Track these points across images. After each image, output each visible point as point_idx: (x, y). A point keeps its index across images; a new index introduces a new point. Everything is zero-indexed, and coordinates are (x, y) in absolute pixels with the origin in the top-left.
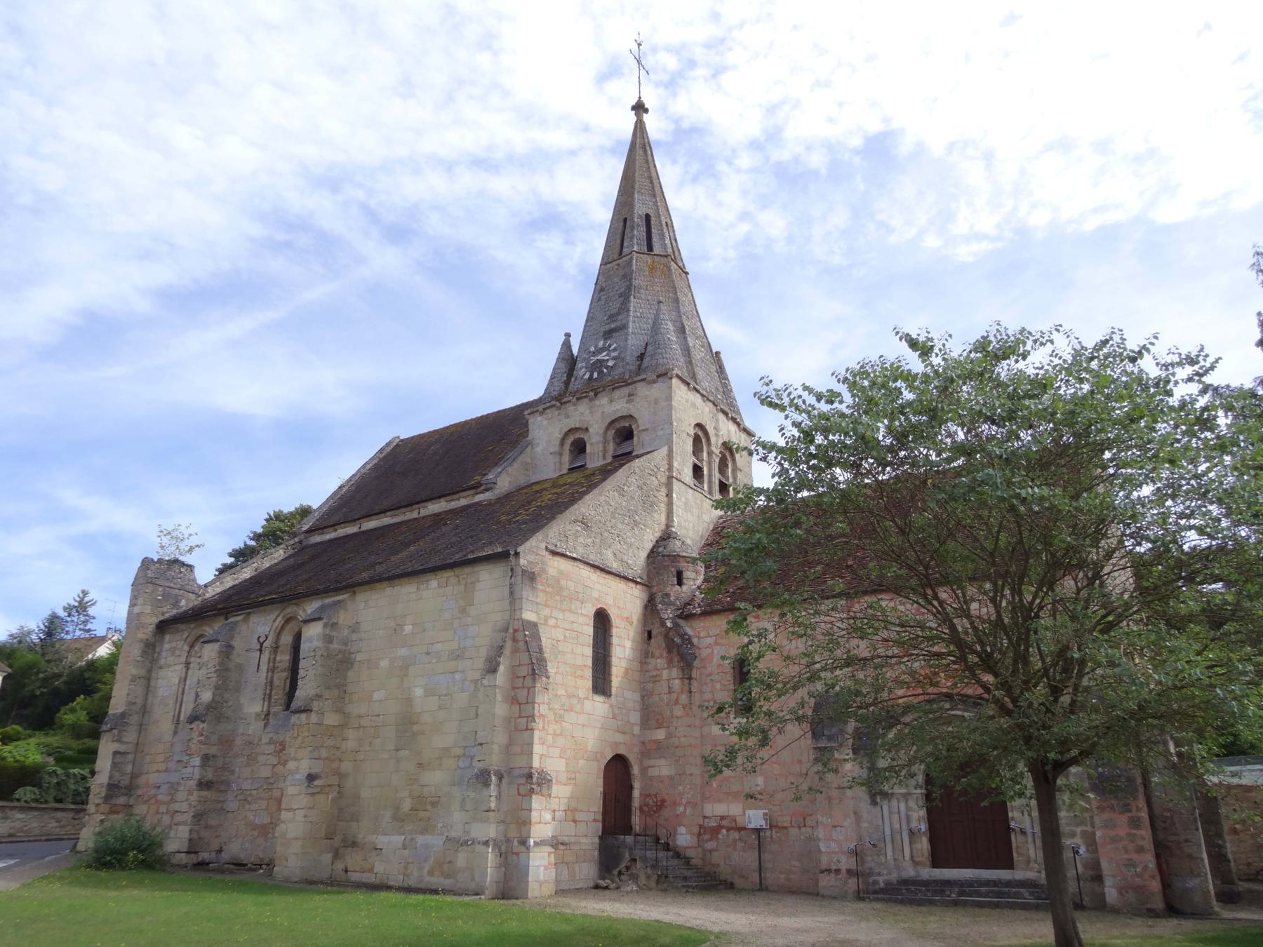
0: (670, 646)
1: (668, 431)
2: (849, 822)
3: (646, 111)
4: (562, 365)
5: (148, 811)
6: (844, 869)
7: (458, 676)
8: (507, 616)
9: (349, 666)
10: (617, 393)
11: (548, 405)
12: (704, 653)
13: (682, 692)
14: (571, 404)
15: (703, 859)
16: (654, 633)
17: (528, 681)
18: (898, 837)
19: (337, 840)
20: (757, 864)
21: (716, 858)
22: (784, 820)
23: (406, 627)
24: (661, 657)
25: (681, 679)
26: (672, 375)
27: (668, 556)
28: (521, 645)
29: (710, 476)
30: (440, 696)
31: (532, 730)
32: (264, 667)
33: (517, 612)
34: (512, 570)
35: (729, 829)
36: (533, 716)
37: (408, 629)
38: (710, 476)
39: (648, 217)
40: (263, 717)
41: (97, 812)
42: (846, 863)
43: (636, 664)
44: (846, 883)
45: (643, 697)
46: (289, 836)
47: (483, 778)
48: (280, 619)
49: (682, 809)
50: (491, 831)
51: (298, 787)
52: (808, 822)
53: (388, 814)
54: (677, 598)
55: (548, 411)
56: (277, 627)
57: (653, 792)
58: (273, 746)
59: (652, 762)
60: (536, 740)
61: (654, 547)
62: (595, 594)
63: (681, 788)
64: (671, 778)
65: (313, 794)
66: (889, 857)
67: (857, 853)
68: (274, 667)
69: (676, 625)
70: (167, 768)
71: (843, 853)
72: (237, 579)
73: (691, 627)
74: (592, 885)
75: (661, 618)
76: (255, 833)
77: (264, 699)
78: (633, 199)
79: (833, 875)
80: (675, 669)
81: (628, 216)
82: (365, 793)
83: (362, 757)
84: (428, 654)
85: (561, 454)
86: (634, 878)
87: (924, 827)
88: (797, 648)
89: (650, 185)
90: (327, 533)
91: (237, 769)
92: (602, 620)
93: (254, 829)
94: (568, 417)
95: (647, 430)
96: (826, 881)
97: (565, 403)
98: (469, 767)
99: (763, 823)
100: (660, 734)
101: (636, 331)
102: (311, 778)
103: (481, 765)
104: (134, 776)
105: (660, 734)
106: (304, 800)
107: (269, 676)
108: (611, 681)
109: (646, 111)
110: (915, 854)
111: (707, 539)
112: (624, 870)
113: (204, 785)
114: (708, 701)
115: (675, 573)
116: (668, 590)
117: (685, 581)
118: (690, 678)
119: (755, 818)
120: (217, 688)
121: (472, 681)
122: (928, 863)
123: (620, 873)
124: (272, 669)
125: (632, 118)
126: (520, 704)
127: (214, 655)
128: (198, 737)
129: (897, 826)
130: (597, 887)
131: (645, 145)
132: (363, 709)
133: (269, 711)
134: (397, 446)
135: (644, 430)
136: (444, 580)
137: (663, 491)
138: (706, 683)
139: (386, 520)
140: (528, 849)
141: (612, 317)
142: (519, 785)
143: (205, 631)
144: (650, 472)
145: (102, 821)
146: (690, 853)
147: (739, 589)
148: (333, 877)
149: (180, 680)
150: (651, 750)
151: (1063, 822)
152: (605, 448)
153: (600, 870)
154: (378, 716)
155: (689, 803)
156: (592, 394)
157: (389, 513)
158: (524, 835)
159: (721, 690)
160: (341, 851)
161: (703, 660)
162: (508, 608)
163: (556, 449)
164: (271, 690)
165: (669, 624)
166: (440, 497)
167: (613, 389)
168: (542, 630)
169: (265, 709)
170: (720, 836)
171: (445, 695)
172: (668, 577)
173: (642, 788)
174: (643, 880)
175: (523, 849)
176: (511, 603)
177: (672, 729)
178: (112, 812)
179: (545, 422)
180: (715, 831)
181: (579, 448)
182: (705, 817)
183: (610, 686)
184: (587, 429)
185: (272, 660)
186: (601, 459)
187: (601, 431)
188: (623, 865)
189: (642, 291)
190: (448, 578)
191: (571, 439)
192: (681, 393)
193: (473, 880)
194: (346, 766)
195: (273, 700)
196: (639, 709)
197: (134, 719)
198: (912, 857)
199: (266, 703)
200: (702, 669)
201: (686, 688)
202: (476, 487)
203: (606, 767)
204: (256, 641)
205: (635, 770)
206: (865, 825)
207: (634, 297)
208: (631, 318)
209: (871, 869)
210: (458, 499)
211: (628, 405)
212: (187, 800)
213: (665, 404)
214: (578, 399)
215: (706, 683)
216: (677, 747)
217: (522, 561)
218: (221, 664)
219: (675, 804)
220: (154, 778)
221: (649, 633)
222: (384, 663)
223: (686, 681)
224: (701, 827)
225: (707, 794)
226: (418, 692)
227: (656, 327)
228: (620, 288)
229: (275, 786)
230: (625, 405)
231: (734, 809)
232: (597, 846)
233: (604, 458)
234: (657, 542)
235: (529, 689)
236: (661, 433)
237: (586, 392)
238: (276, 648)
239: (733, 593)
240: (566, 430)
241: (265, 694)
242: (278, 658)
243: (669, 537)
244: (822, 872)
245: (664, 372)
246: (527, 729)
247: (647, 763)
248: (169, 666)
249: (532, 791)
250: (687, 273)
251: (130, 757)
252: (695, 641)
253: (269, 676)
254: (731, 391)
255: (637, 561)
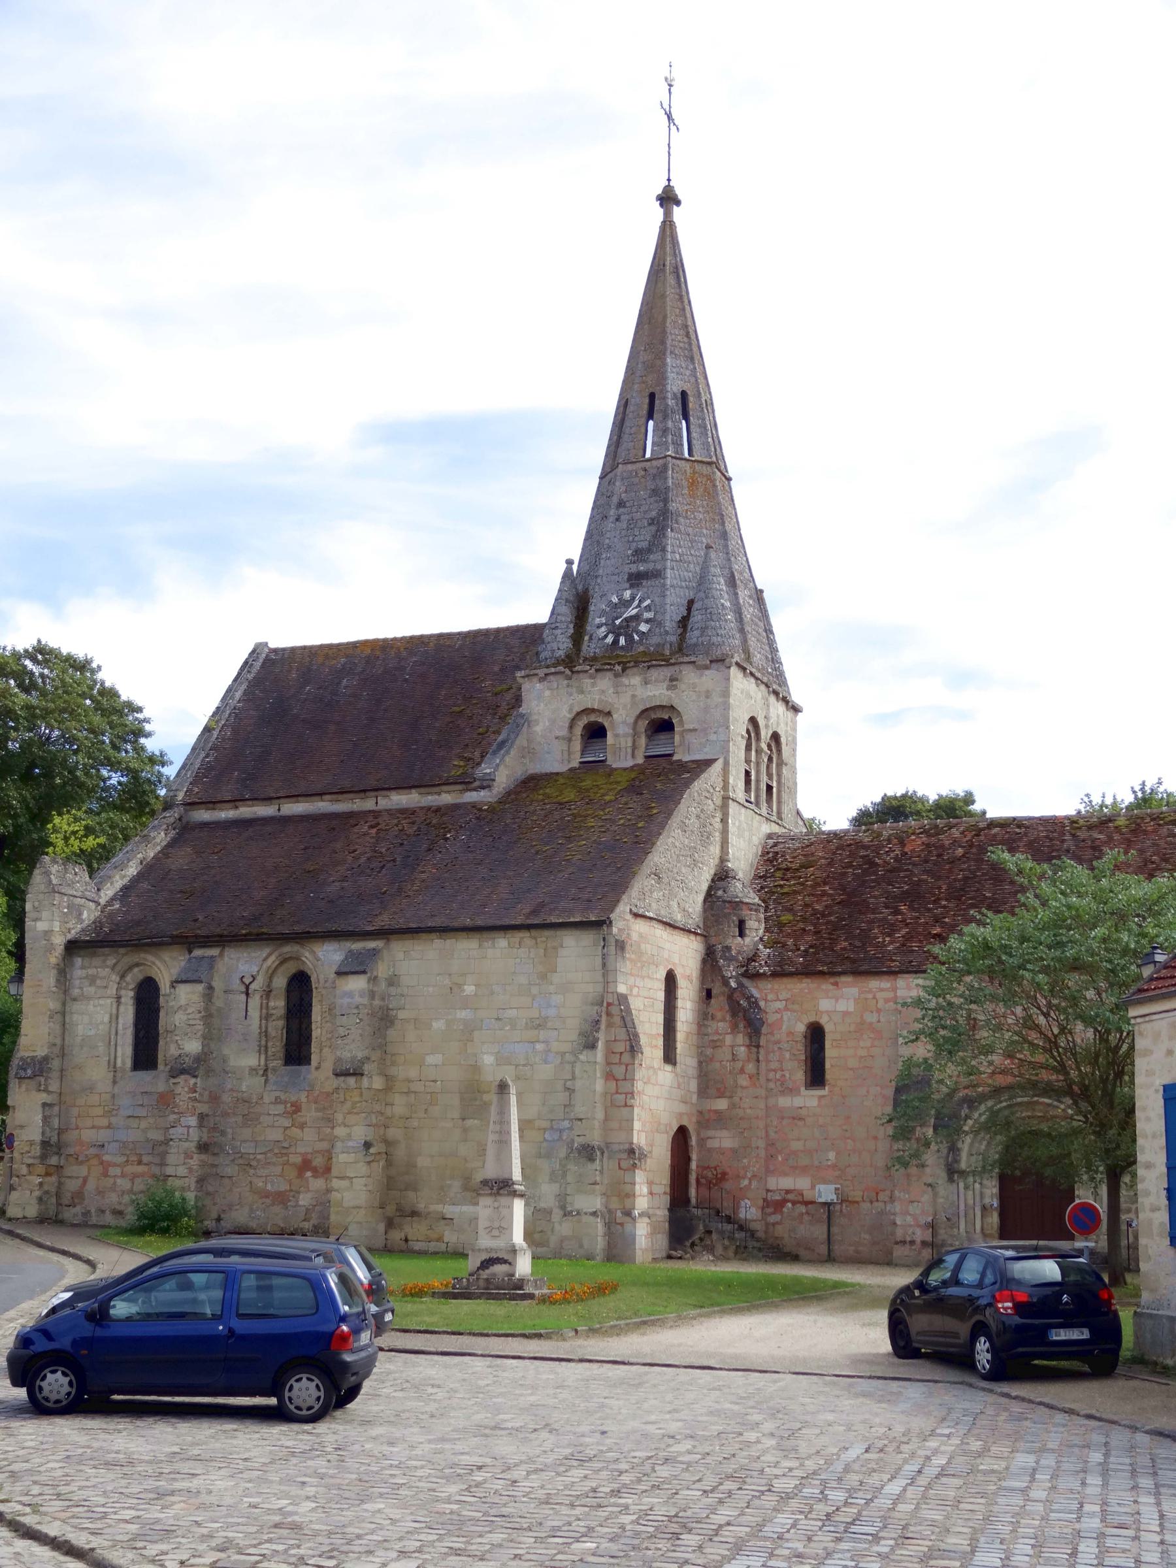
0: (735, 1009)
1: (722, 737)
2: (926, 1198)
3: (678, 203)
4: (564, 609)
5: (89, 1173)
6: (918, 1241)
7: (540, 1047)
8: (599, 988)
9: (388, 1024)
10: (654, 674)
11: (553, 670)
12: (771, 1018)
13: (749, 1061)
14: (585, 675)
15: (766, 1232)
16: (714, 992)
17: (626, 1058)
18: (971, 1212)
19: (391, 1210)
20: (825, 1236)
21: (780, 1231)
22: (857, 1195)
23: (466, 987)
24: (723, 1020)
25: (748, 1046)
26: (731, 663)
27: (730, 902)
28: (617, 1020)
29: (758, 781)
30: (517, 1066)
31: (632, 1106)
32: (255, 1013)
33: (611, 985)
34: (604, 939)
35: (794, 1203)
36: (632, 1093)
37: (469, 989)
38: (758, 781)
39: (684, 394)
40: (261, 1072)
41: (30, 1173)
42: (920, 1235)
43: (695, 1027)
44: (920, 1253)
45: (700, 1063)
46: (345, 1204)
47: (588, 1152)
48: (273, 958)
49: (746, 1182)
50: (596, 1202)
51: (353, 1155)
52: (881, 1196)
53: (456, 1185)
54: (739, 953)
55: (551, 677)
56: (269, 968)
57: (712, 1165)
58: (282, 1106)
59: (711, 1133)
60: (635, 1117)
61: (710, 888)
62: (666, 956)
63: (745, 1161)
64: (734, 1151)
65: (369, 1163)
66: (961, 1230)
67: (932, 1226)
68: (267, 1014)
69: (740, 985)
70: (110, 1124)
71: (919, 1226)
72: (124, 876)
73: (757, 987)
74: (664, 1255)
75: (723, 977)
76: (268, 1201)
77: (260, 1052)
78: (665, 364)
79: (908, 1246)
80: (741, 1035)
81: (657, 390)
82: (422, 1162)
83: (416, 1124)
84: (498, 1019)
85: (570, 740)
86: (711, 1249)
87: (996, 1203)
88: (879, 1021)
89: (686, 340)
90: (222, 810)
91: (229, 1131)
92: (671, 980)
93: (267, 1197)
94: (582, 692)
95: (695, 730)
96: (899, 1252)
97: (578, 672)
98: (558, 1140)
99: (834, 1197)
100: (722, 1104)
101: (675, 582)
102: (367, 1145)
103: (581, 1140)
104: (61, 1132)
105: (722, 1104)
106: (363, 1169)
107: (263, 1026)
108: (676, 1048)
109: (678, 203)
110: (985, 1226)
111: (757, 869)
112: (697, 1242)
113: (203, 1147)
114: (775, 1071)
115: (737, 923)
116: (729, 942)
117: (747, 932)
118: (758, 1046)
119: (826, 1193)
120: (204, 1037)
121: (557, 1053)
122: (997, 1235)
123: (693, 1245)
124: (265, 1016)
125: (659, 213)
126: (617, 1080)
127: (196, 998)
128: (188, 1093)
129: (971, 1202)
130: (670, 1257)
131: (677, 268)
132: (413, 1073)
133: (266, 1065)
134: (267, 660)
135: (690, 730)
136: (517, 940)
137: (719, 815)
138: (773, 1052)
139: (323, 806)
140: (634, 1219)
141: (640, 554)
142: (620, 1160)
143: (146, 960)
144: (707, 795)
145: (41, 1184)
146: (754, 1226)
147: (811, 947)
148: (389, 1246)
149: (111, 1018)
150: (718, 1120)
151: (1122, 1199)
152: (634, 742)
153: (670, 1242)
154: (435, 1081)
155: (754, 1176)
156: (618, 668)
157: (328, 797)
158: (628, 1206)
159: (790, 1059)
160: (397, 1220)
161: (770, 1025)
162: (601, 979)
163: (564, 732)
164: (267, 1041)
165: (733, 984)
166: (411, 787)
167: (649, 667)
168: (631, 1000)
169: (263, 1062)
170: (785, 1210)
171: (524, 1065)
172: (729, 926)
173: (698, 1160)
174: (719, 1250)
175: (628, 1219)
176: (604, 975)
177: (736, 1099)
178: (48, 1174)
179: (547, 693)
180: (779, 1205)
181: (596, 733)
182: (768, 1191)
183: (675, 1054)
184: (609, 714)
185: (264, 1005)
186: (629, 756)
187: (631, 720)
188: (696, 1237)
189: (681, 520)
190: (523, 938)
191: (584, 721)
192: (740, 684)
193: (581, 1246)
194: (393, 1133)
195: (270, 1053)
196: (696, 1075)
197: (55, 1064)
198: (982, 1229)
199: (263, 1057)
200: (769, 1036)
201: (754, 1056)
202: (466, 782)
203: (673, 1139)
204: (238, 982)
205: (694, 1141)
206: (941, 1200)
207: (672, 530)
208: (669, 563)
209: (943, 1240)
210: (439, 794)
211: (669, 693)
212: (184, 1164)
213: (720, 700)
214: (597, 670)
215: (773, 1052)
216: (741, 1119)
217: (615, 930)
218: (206, 1009)
219: (738, 1177)
220: (88, 1135)
221: (709, 994)
222: (439, 1025)
223: (754, 1050)
224: (765, 1200)
225: (772, 1168)
226: (488, 1060)
227: (703, 580)
228: (650, 510)
229: (292, 1150)
230: (665, 692)
231: (802, 1183)
232: (667, 1218)
233: (633, 756)
234: (713, 880)
235: (627, 1066)
236: (713, 737)
237: (609, 664)
238: (268, 993)
239: (806, 951)
240: (577, 709)
241: (260, 1046)
242: (272, 1004)
243: (727, 877)
244: (897, 1243)
245: (720, 657)
246: (626, 1105)
247: (704, 1134)
248: (89, 998)
249: (634, 1166)
250: (729, 479)
251: (56, 1109)
252: (762, 1004)
253: (263, 1026)
254: (777, 651)
255: (695, 903)
